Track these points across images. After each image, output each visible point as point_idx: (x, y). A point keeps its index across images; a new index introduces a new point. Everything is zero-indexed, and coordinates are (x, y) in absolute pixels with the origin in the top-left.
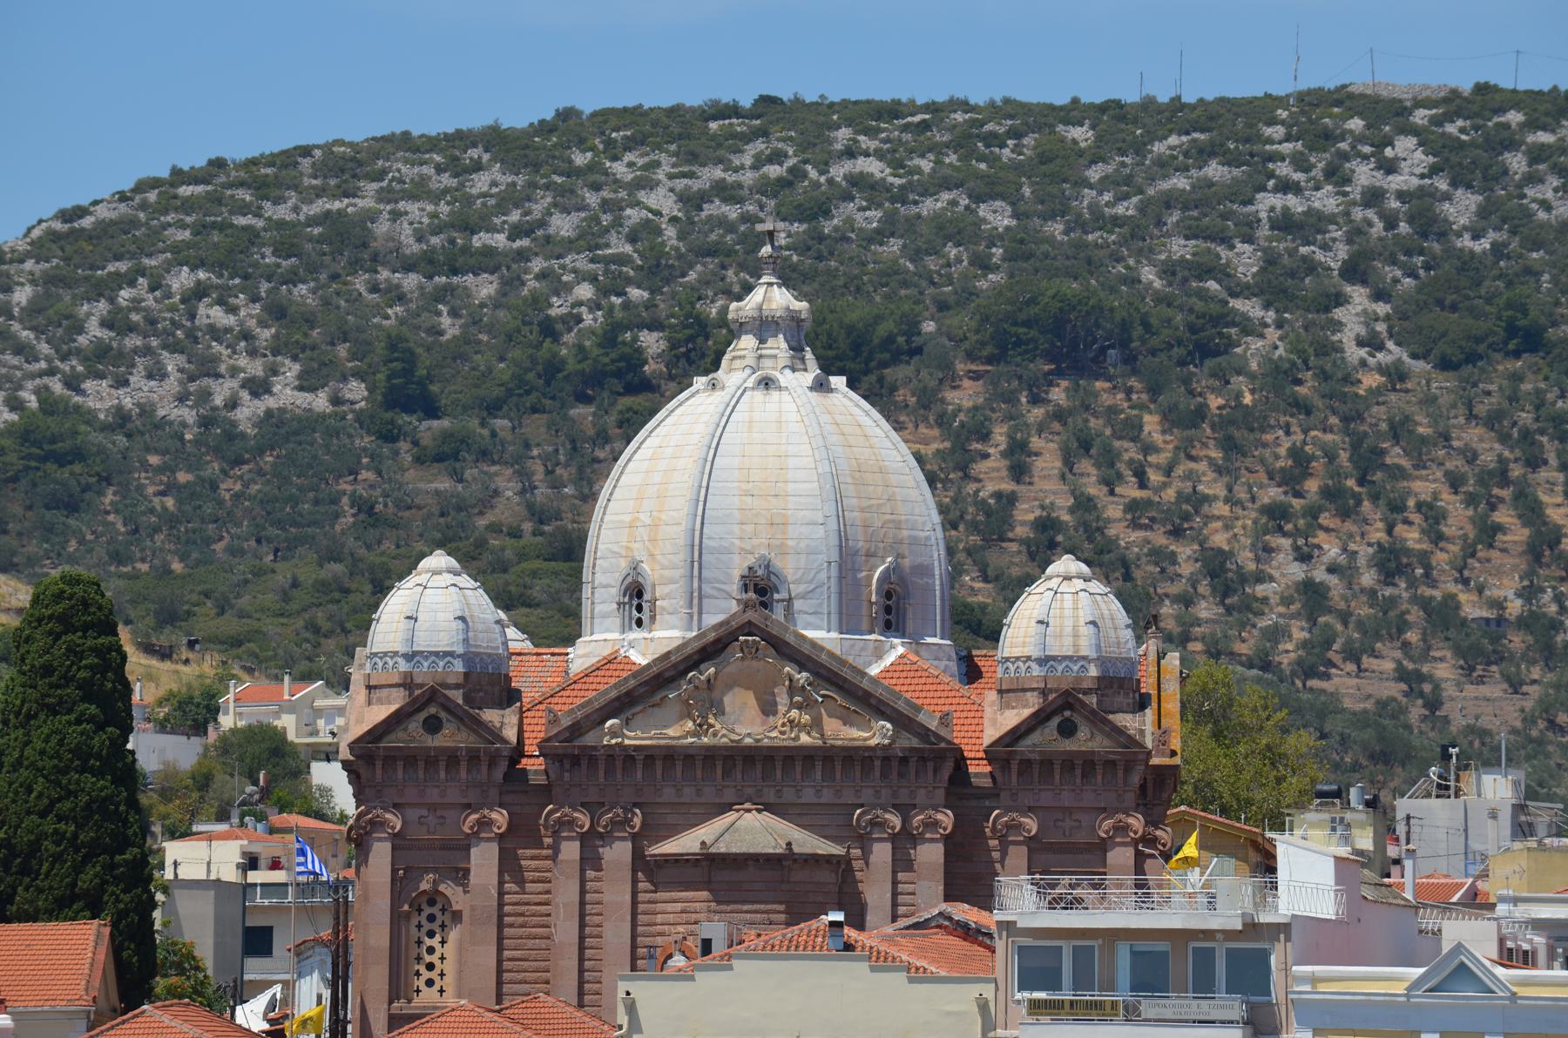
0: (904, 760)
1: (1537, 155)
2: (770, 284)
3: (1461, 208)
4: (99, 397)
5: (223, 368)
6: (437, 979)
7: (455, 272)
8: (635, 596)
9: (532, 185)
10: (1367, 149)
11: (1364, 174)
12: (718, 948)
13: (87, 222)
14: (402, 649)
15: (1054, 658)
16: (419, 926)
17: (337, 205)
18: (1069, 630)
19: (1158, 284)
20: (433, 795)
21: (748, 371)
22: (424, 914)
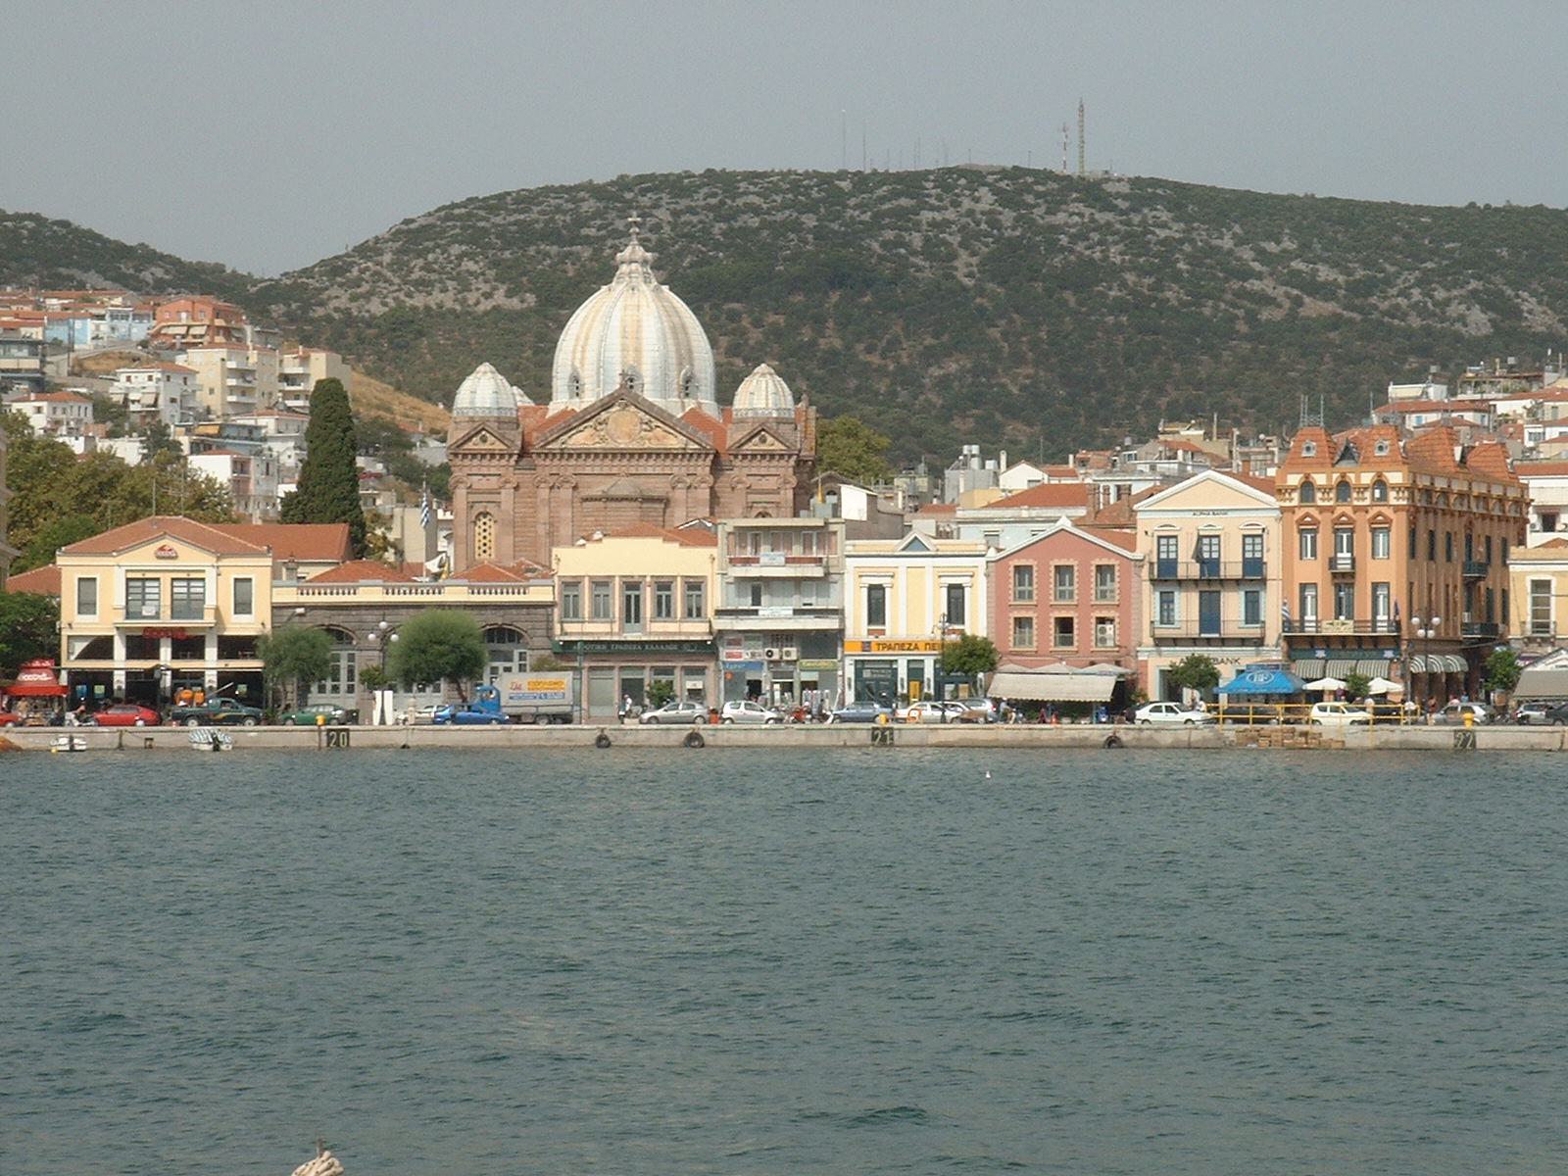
0: (691, 454)
1: (1038, 195)
3: (1007, 216)
4: (419, 301)
5: (473, 287)
7: (572, 245)
8: (576, 384)
9: (606, 208)
10: (967, 192)
11: (967, 204)
13: (412, 226)
14: (469, 406)
17: (522, 217)
19: (880, 251)
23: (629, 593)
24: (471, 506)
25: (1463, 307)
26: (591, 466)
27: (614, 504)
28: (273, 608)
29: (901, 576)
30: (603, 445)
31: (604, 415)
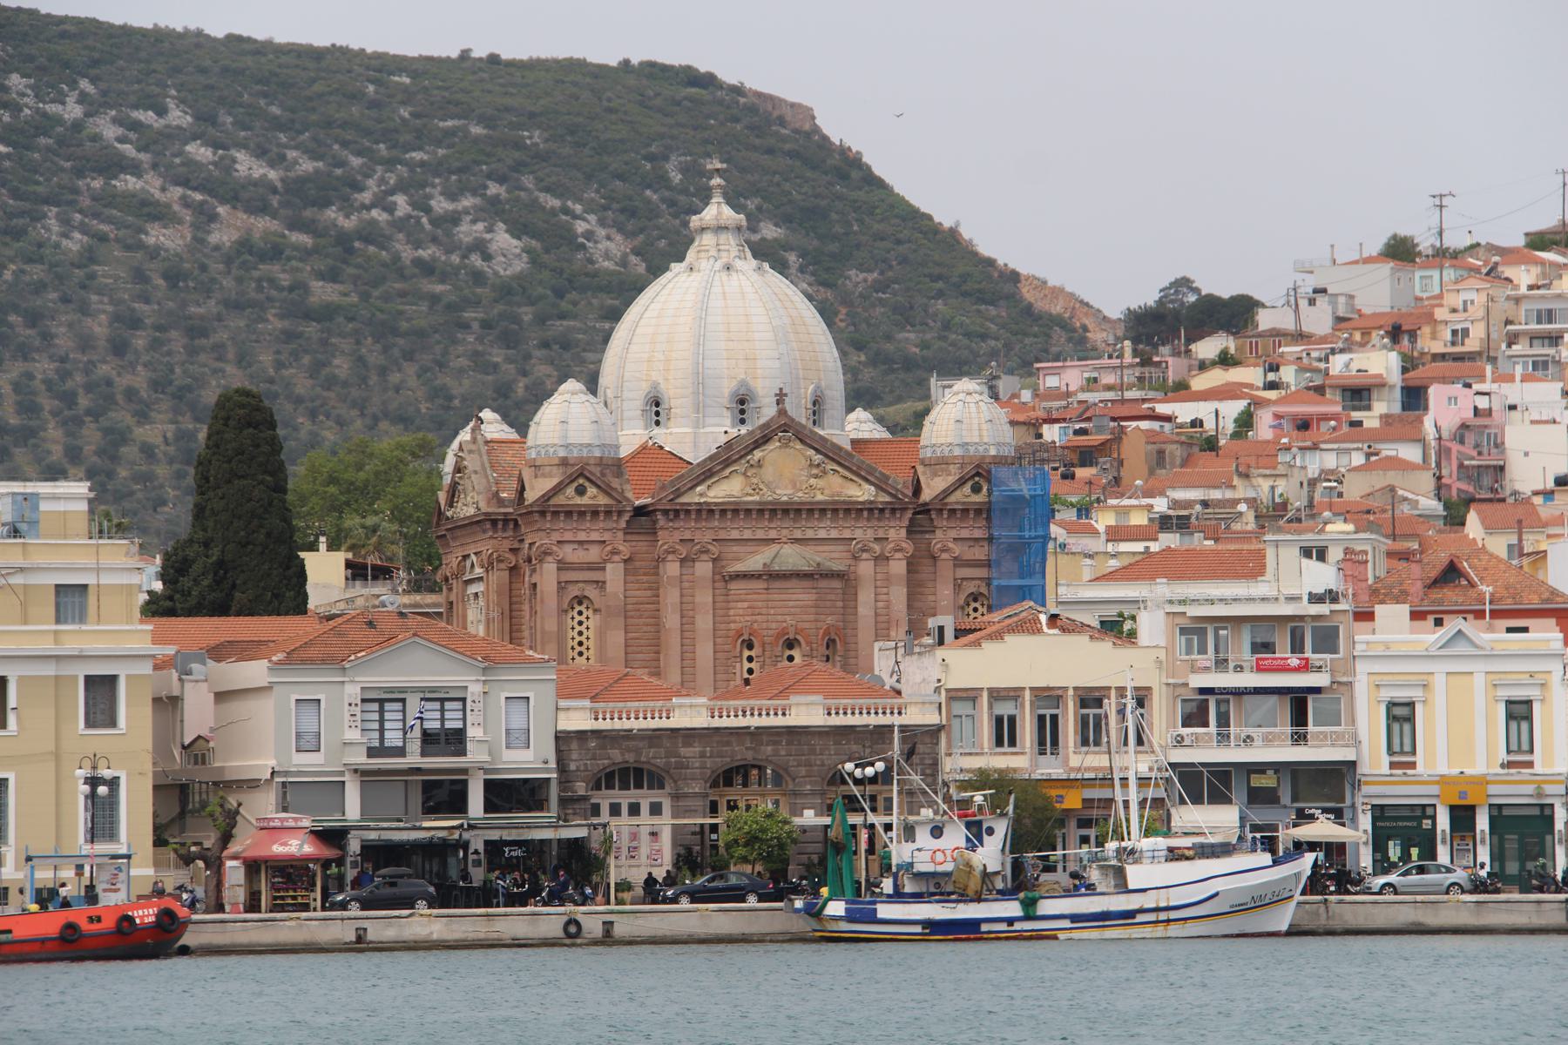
2: (719, 203)
6: (585, 651)
12: (949, 634)
15: (967, 444)
16: (573, 618)
18: (975, 427)
20: (582, 536)
21: (712, 260)
22: (576, 611)
23: (1042, 712)
24: (562, 586)
25: (480, 226)
26: (736, 530)
27: (778, 584)
28: (557, 738)
29: (1439, 682)
30: (756, 498)
31: (758, 454)
